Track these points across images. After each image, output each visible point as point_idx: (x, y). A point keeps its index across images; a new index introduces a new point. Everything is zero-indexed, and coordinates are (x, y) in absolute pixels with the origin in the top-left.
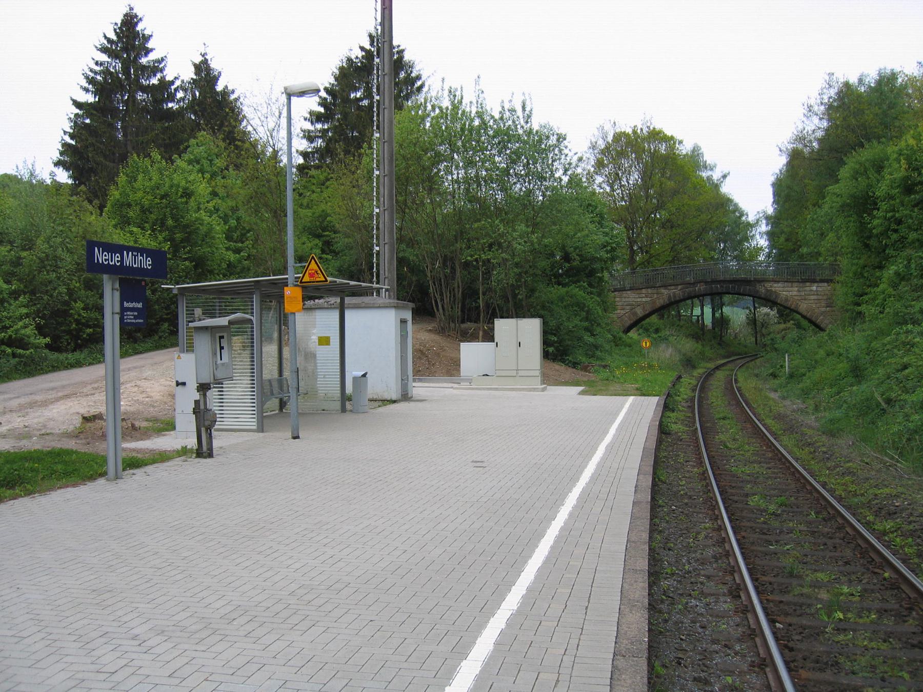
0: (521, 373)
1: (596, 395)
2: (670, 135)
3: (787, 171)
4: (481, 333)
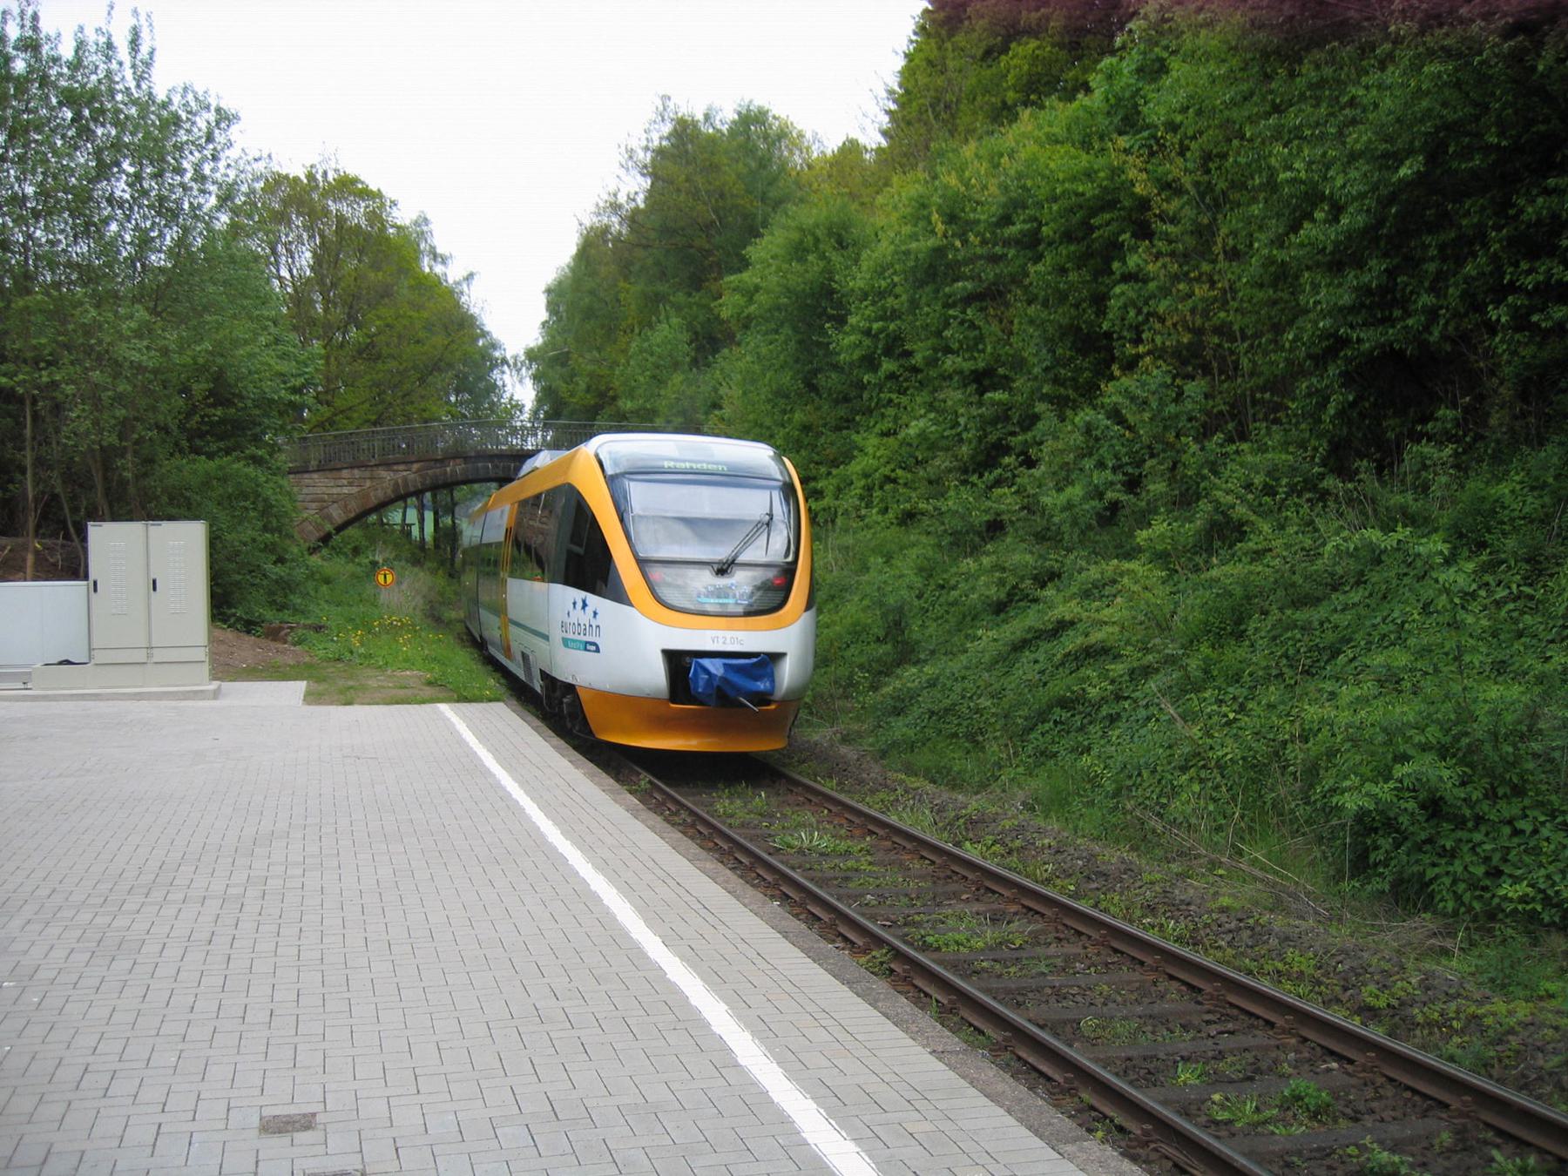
0: (158, 656)
2: (375, 189)
3: (572, 270)
4: (30, 558)
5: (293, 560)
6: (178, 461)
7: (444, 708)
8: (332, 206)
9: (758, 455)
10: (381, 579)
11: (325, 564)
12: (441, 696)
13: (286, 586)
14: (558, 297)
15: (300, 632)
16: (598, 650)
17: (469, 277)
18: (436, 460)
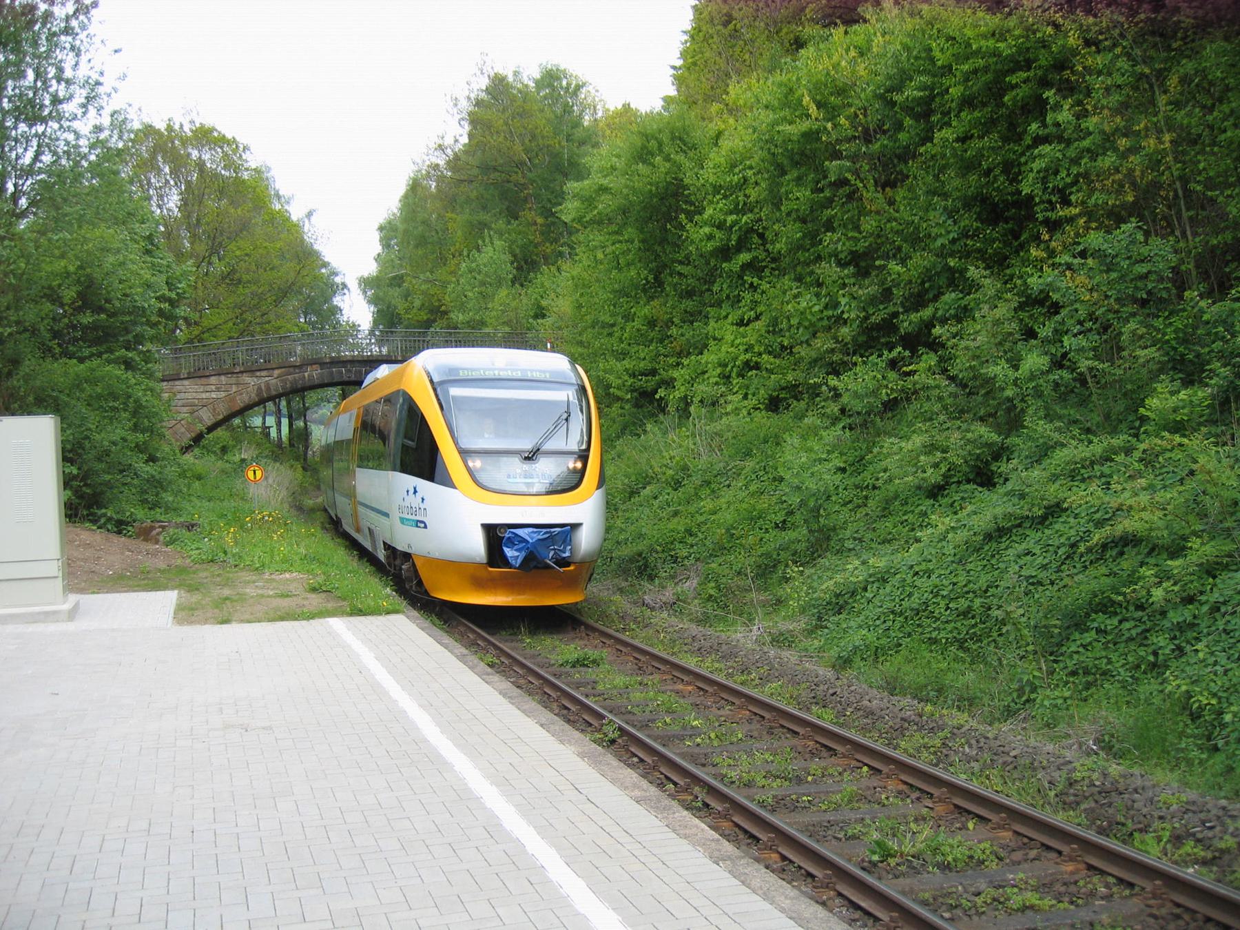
1: (226, 621)
5: (164, 459)
6: (49, 364)
7: (337, 624)
8: (195, 154)
9: (556, 363)
10: (251, 474)
11: (196, 461)
12: (330, 605)
13: (158, 484)
14: (388, 231)
15: (171, 531)
16: (425, 527)
17: (309, 215)
18: (295, 367)
